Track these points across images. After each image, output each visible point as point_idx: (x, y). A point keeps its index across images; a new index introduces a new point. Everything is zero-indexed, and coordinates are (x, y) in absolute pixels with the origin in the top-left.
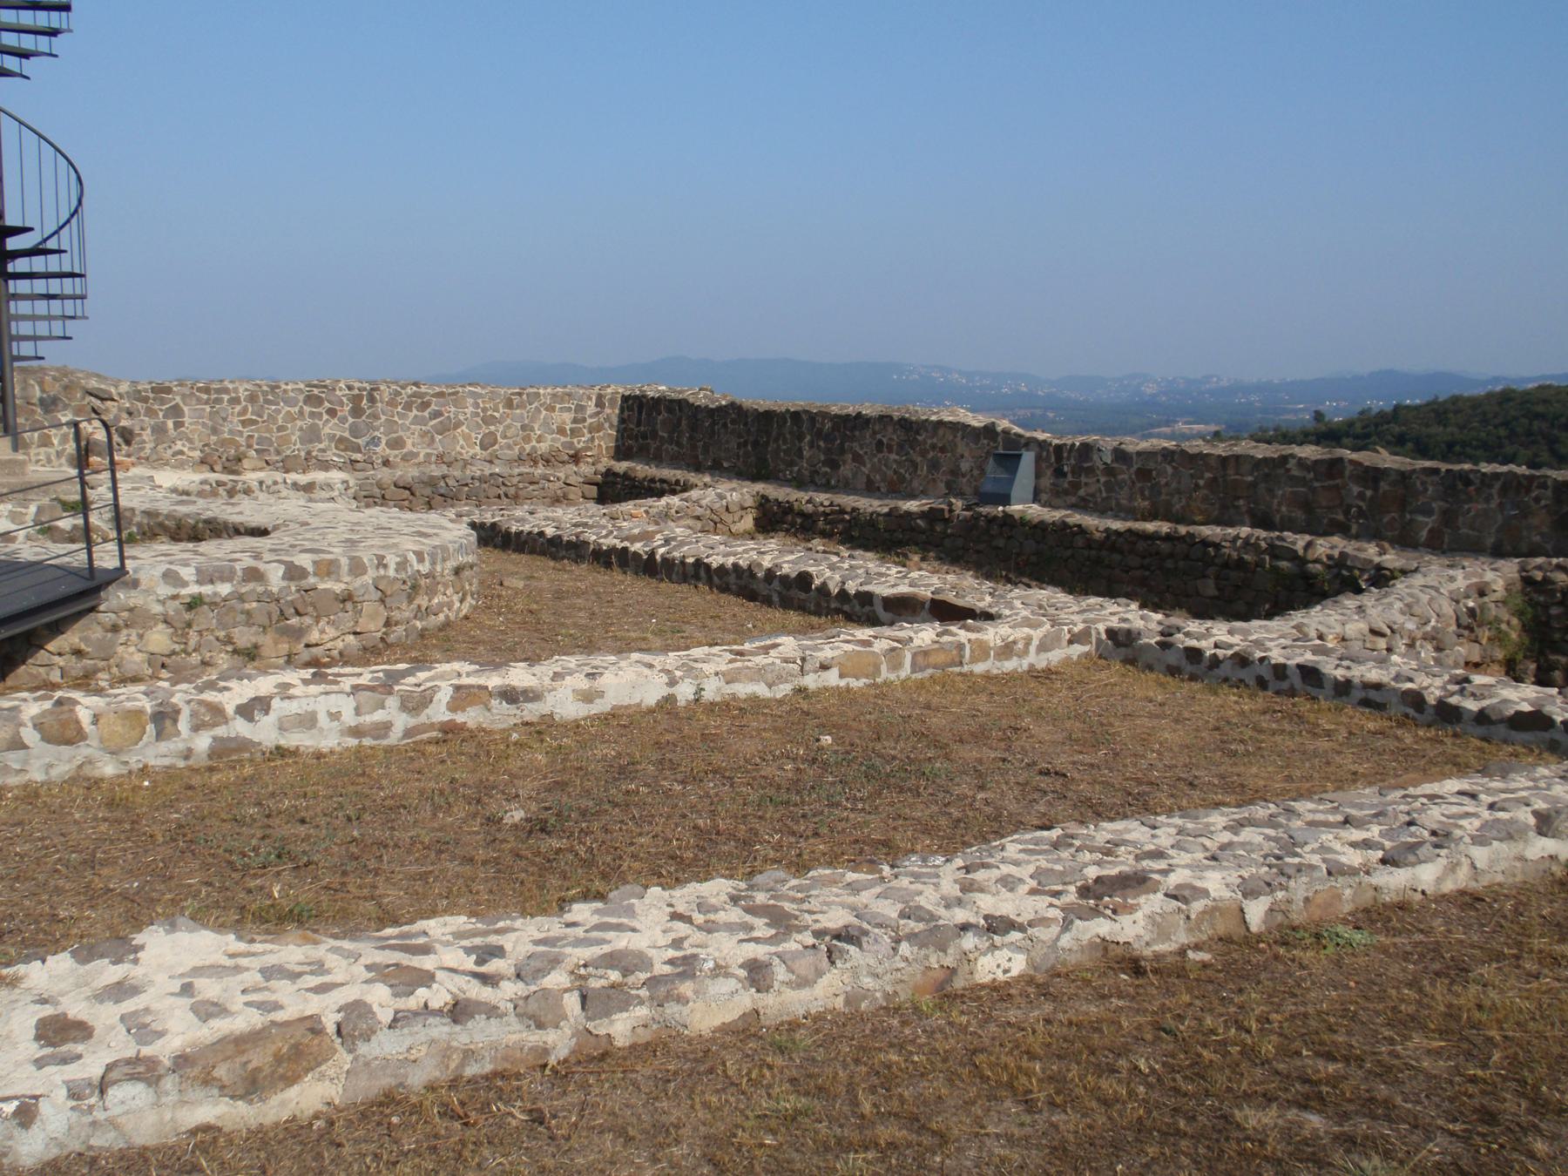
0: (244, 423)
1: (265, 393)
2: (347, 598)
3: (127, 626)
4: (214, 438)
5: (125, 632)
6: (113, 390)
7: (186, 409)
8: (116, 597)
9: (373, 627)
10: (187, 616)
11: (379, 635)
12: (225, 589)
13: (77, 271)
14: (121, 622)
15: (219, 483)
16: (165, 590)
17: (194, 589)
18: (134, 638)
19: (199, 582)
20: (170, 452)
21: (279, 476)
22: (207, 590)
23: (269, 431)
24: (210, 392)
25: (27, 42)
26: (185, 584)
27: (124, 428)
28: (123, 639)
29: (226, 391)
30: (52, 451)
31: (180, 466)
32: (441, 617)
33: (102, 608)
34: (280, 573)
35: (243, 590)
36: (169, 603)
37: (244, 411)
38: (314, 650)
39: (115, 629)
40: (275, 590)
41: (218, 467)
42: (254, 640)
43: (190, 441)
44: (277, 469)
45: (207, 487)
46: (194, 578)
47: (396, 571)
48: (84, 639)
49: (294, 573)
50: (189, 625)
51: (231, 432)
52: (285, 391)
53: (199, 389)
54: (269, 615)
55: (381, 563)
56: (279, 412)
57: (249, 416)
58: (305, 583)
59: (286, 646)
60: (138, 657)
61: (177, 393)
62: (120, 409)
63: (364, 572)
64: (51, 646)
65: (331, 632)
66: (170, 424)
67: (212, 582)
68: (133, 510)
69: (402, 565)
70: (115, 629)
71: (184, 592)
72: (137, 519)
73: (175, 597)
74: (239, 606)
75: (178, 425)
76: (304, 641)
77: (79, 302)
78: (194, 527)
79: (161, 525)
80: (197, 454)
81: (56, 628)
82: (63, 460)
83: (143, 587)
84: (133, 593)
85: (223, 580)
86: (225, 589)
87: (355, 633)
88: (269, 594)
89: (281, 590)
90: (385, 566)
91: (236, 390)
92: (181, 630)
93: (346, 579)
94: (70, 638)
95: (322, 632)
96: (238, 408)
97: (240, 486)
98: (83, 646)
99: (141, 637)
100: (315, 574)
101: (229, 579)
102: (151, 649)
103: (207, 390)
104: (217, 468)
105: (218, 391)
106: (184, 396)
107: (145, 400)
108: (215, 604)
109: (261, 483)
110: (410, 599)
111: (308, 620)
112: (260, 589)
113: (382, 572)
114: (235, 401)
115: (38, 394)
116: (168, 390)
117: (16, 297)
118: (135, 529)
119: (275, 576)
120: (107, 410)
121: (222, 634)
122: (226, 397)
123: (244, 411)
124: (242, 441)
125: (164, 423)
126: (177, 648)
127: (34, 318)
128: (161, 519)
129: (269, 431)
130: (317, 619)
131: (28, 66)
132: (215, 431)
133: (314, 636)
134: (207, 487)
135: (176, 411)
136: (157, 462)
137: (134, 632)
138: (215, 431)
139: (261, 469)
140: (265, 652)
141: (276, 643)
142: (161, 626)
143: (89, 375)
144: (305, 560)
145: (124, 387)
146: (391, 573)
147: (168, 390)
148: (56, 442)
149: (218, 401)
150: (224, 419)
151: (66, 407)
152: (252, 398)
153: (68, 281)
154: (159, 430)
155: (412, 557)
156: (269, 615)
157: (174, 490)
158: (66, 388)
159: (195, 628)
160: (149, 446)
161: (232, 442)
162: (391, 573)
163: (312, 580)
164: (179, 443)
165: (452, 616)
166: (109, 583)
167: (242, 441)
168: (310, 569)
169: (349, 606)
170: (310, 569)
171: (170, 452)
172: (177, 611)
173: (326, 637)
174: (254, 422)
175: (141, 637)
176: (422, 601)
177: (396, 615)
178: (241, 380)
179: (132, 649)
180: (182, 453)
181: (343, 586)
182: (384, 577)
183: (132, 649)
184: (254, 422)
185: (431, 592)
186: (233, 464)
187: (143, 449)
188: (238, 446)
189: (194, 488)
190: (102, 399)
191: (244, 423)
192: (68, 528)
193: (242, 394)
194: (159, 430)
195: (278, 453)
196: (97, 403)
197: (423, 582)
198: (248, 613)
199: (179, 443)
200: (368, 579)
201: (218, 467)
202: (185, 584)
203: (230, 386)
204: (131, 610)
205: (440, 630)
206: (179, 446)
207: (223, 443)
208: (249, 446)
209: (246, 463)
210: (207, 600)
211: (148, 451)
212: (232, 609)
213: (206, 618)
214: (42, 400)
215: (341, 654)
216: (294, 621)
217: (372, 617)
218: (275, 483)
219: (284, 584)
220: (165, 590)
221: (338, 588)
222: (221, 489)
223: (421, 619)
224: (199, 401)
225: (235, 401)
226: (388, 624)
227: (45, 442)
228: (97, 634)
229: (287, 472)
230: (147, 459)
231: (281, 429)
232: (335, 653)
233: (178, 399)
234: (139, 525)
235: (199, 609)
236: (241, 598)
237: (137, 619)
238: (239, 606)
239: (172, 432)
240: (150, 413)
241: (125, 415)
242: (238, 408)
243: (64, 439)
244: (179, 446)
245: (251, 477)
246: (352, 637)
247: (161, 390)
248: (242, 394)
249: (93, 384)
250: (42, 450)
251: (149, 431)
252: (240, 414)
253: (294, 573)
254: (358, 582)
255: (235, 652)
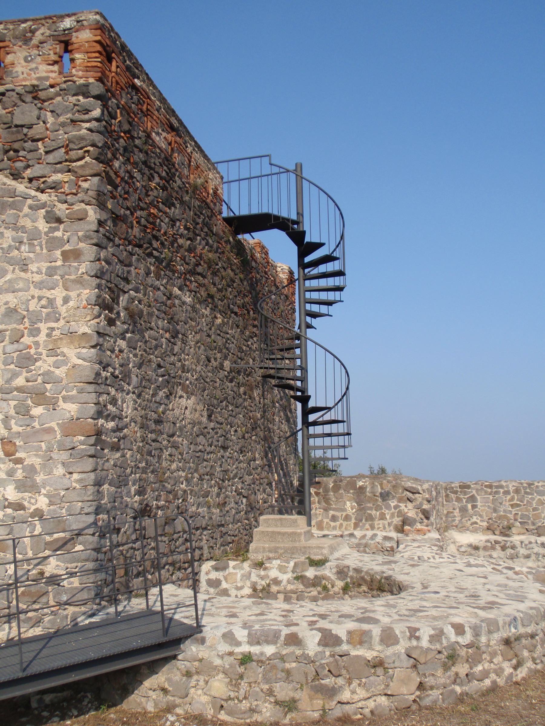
0: (512, 506)
1: (525, 488)
2: (378, 664)
3: (198, 673)
4: (494, 515)
5: (195, 677)
6: (419, 488)
7: (478, 497)
8: (191, 649)
9: (407, 692)
10: (241, 670)
11: (413, 697)
12: (269, 650)
13: (340, 419)
14: (193, 670)
15: (496, 542)
16: (224, 648)
17: (245, 648)
18: (202, 683)
19: (250, 643)
20: (469, 522)
21: (533, 538)
22: (255, 650)
23: (527, 510)
24: (492, 488)
25: (323, 296)
26: (238, 644)
27: (424, 509)
28: (193, 683)
29: (501, 487)
30: (386, 522)
31: (475, 531)
32: (487, 682)
33: (180, 657)
34: (317, 640)
35: (284, 652)
36: (226, 658)
37: (512, 499)
38: (347, 707)
39: (188, 674)
40: (311, 653)
41: (497, 532)
42: (291, 694)
43: (481, 516)
44: (533, 534)
45: (489, 544)
46: (246, 639)
47: (430, 642)
48: (168, 680)
49: (329, 639)
50: (241, 677)
51: (505, 511)
52: (537, 487)
53: (486, 486)
54: (306, 674)
55: (413, 634)
56: (533, 499)
57: (515, 502)
58: (338, 650)
59: (321, 702)
60: (204, 699)
61: (473, 489)
62: (423, 499)
63: (396, 642)
64: (147, 683)
65: (362, 693)
66: (469, 506)
67: (258, 643)
68: (348, 567)
69: (437, 637)
70: (188, 674)
71: (238, 650)
72: (351, 573)
73: (231, 654)
74: (280, 665)
75: (474, 507)
76: (337, 698)
77: (346, 437)
78: (380, 581)
79: (362, 578)
80: (485, 524)
81: (153, 667)
82: (392, 528)
83: (208, 643)
84: (201, 648)
85: (268, 642)
86: (269, 650)
87: (386, 695)
88: (305, 656)
89: (316, 655)
90: (205, 680)
91: (507, 486)
92: (235, 681)
93: (379, 648)
94: (159, 679)
95: (353, 692)
96: (509, 497)
97: (508, 544)
98: (167, 686)
99: (207, 682)
100: (348, 642)
101: (274, 643)
102: (213, 693)
103: (490, 487)
104: (497, 532)
105: (497, 487)
106: (477, 490)
107: (456, 492)
108: (262, 662)
109: (522, 542)
110: (446, 668)
111: (340, 681)
112: (298, 652)
113: (414, 643)
114: (507, 493)
115: (380, 490)
116: (468, 487)
117: (315, 436)
118: (349, 580)
119: (312, 642)
120: (416, 499)
121: (266, 687)
122: (502, 490)
123: (512, 499)
124: (511, 516)
125: (466, 506)
126: (232, 694)
127: (323, 448)
128: (363, 574)
129: (527, 510)
130: (349, 682)
131: (332, 309)
132: (495, 510)
133: (346, 695)
134: (489, 544)
135: (473, 499)
136: (462, 528)
137: (202, 678)
138: (495, 510)
139: (523, 534)
140: (301, 705)
141: (311, 699)
142: (221, 676)
143: (409, 479)
144: (340, 631)
145: (426, 486)
146: (425, 643)
147: (468, 487)
148: (388, 517)
149: (497, 493)
150: (501, 504)
151: (394, 497)
152: (517, 491)
153: (334, 426)
154: (463, 510)
155: (450, 631)
156: (306, 674)
157: (470, 546)
158: (394, 487)
159: (245, 680)
160: (458, 519)
161: (505, 517)
162: (425, 643)
163: (345, 647)
164: (475, 517)
165: (501, 682)
166: (187, 638)
167: (511, 516)
168: (344, 638)
169: (380, 671)
170: (344, 638)
171: (469, 522)
172: (231, 665)
173: (356, 697)
174: (518, 505)
175: (207, 682)
176: (462, 669)
177: (430, 681)
178: (511, 481)
179: (200, 692)
180: (476, 523)
181: (375, 654)
182: (416, 647)
183: (200, 692)
184: (518, 505)
185: (473, 661)
186: (506, 531)
187: (454, 520)
188: (508, 520)
189: (481, 544)
190: (413, 493)
191: (512, 506)
192: (312, 577)
193: (511, 489)
194: (463, 510)
195: (533, 524)
196: (410, 495)
197: (463, 652)
198: (288, 672)
199: (475, 517)
200: (401, 648)
201: (497, 532)
202: (238, 644)
203: (504, 484)
204: (201, 660)
205: (483, 695)
206: (474, 519)
207: (500, 517)
208: (516, 520)
209: (514, 530)
210: (255, 658)
211: (457, 522)
212: (274, 667)
213: (256, 672)
214: (381, 494)
215: (372, 712)
216: (328, 681)
217: (404, 682)
218: (530, 543)
219: (320, 649)
220: (224, 648)
221: (369, 655)
222: (497, 546)
223: (461, 685)
224: (486, 492)
225: (507, 493)
226: (421, 686)
227: (382, 517)
228: (177, 677)
229: (539, 536)
230: (456, 526)
231: (535, 509)
232: (367, 711)
233: (474, 492)
234: (352, 577)
235: (248, 665)
236: (282, 659)
237: (205, 669)
238: (280, 665)
239: (470, 511)
240: (458, 500)
241: (425, 502)
242: (509, 497)
243: (392, 516)
244: (474, 519)
245: (516, 539)
246: (384, 698)
247: (464, 487)
248: (511, 489)
249: (409, 484)
250: (381, 522)
251: (458, 510)
252: (510, 501)
253: (329, 639)
254: (390, 651)
255: (277, 703)
